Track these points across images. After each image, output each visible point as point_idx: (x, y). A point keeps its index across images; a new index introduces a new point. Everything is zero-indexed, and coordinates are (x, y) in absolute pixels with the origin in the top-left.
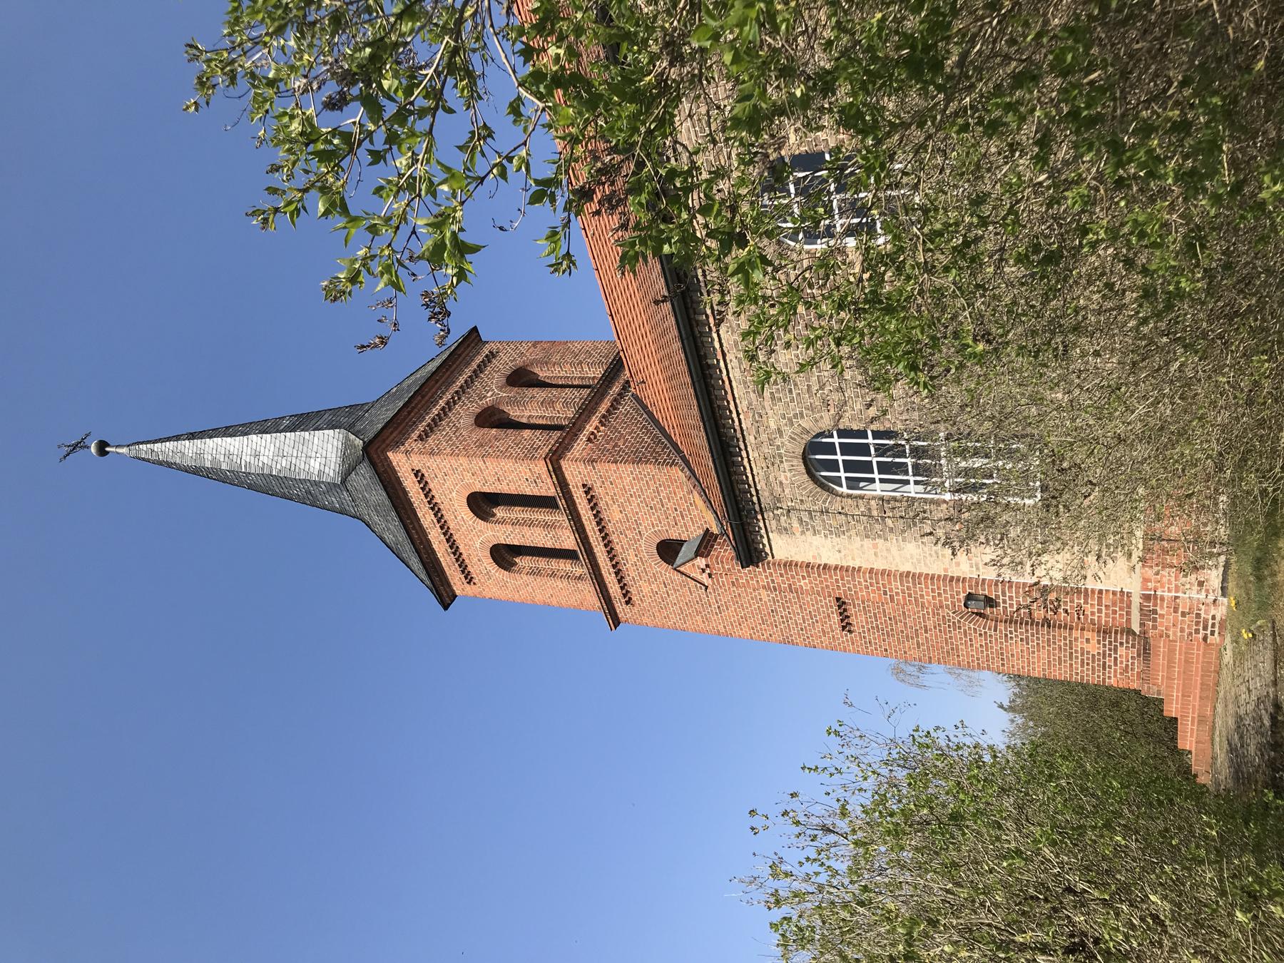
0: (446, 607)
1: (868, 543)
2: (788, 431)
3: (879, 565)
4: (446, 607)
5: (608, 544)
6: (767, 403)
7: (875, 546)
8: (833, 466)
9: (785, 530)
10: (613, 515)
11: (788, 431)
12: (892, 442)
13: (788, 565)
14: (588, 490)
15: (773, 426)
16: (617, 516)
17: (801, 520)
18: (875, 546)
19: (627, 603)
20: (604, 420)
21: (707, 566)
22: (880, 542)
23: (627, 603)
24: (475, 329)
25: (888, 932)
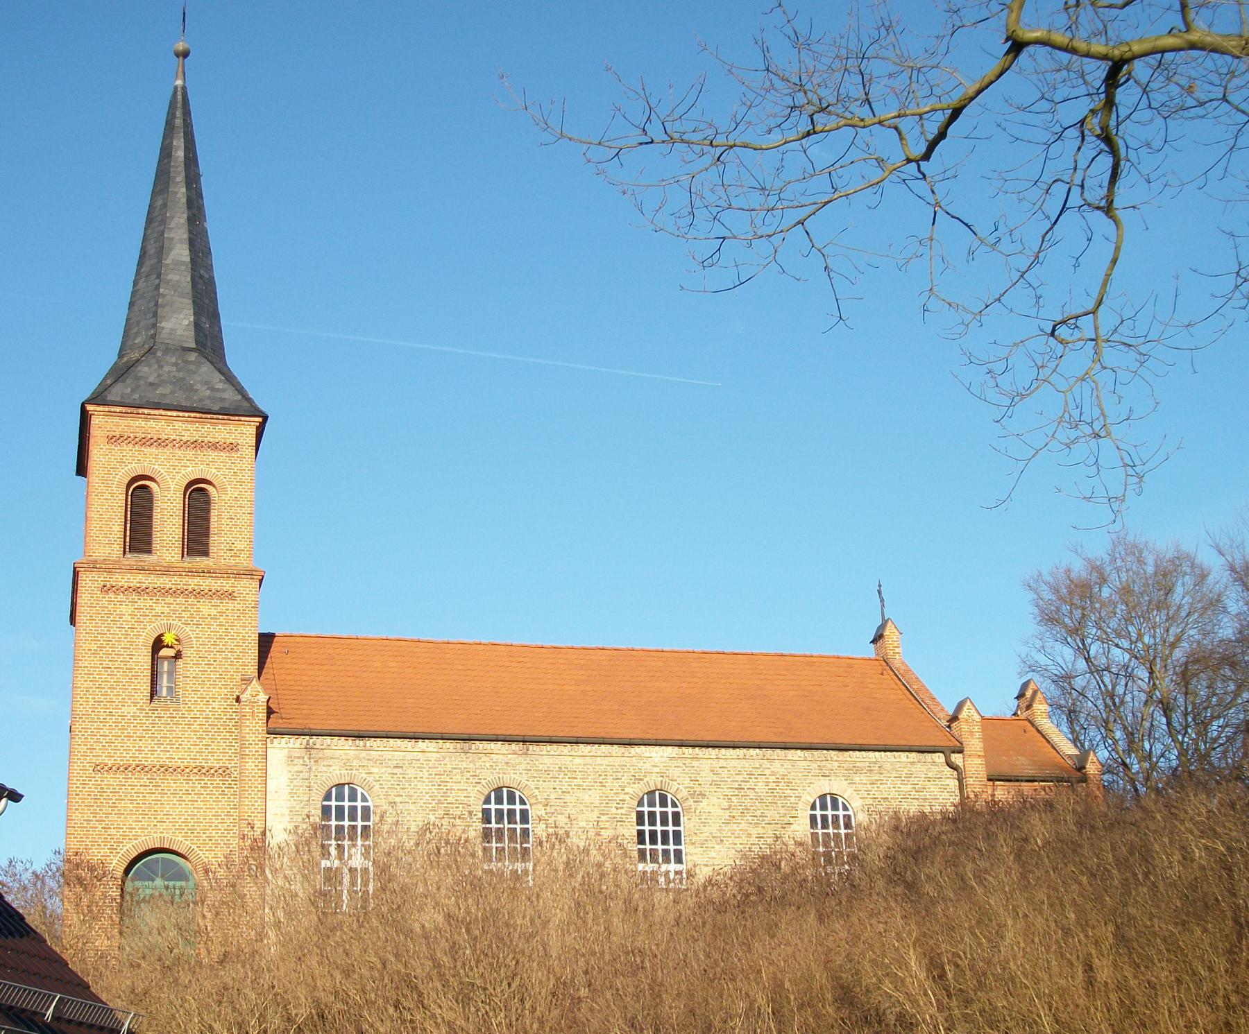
6: (390, 770)
7: (283, 815)
9: (291, 759)
10: (206, 608)
11: (370, 778)
14: (231, 595)
18: (283, 815)
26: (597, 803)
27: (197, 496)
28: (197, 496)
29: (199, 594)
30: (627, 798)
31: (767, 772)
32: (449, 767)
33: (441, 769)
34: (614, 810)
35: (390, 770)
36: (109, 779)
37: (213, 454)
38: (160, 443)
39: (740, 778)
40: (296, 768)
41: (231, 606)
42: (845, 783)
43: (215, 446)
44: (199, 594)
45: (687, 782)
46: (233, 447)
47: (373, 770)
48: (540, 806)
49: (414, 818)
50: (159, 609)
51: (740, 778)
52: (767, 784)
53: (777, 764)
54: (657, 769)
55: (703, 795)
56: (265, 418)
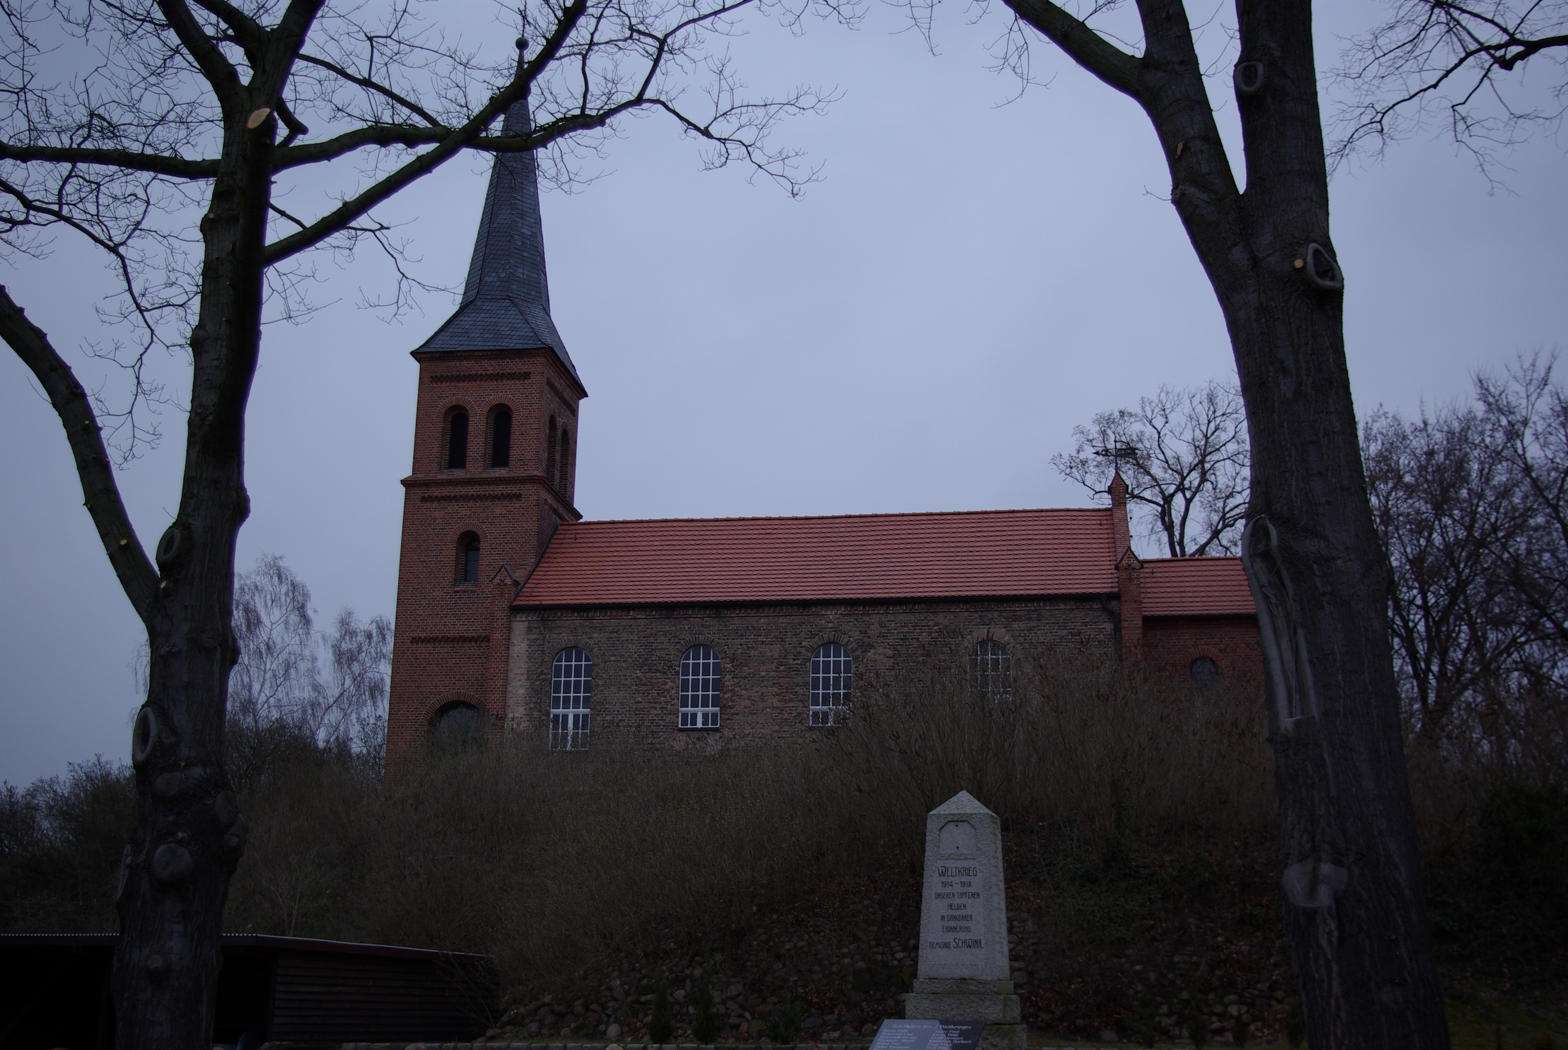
0: (412, 353)
1: (524, 671)
2: (591, 642)
3: (511, 675)
4: (412, 353)
5: (475, 498)
6: (607, 635)
7: (522, 674)
8: (568, 659)
9: (530, 630)
10: (499, 508)
11: (591, 642)
12: (1399, 920)
13: (510, 629)
14: (518, 497)
15: (595, 635)
16: (498, 511)
17: (537, 639)
18: (522, 674)
19: (424, 497)
20: (551, 507)
21: (506, 584)
22: (525, 677)
23: (424, 497)
24: (587, 396)
25: (721, 737)
26: (776, 655)
27: (501, 417)
28: (501, 417)
29: (494, 498)
30: (803, 650)
31: (931, 623)
32: (654, 631)
33: (648, 631)
34: (791, 661)
35: (607, 635)
36: (421, 648)
37: (510, 382)
38: (471, 378)
39: (906, 630)
40: (534, 637)
41: (517, 504)
42: (1003, 630)
43: (513, 376)
44: (494, 498)
45: (857, 635)
46: (526, 376)
47: (595, 635)
48: (728, 660)
49: (268, 714)
50: (463, 512)
51: (906, 630)
52: (930, 634)
53: (941, 616)
54: (831, 625)
55: (871, 646)
56: (1453, 107)
